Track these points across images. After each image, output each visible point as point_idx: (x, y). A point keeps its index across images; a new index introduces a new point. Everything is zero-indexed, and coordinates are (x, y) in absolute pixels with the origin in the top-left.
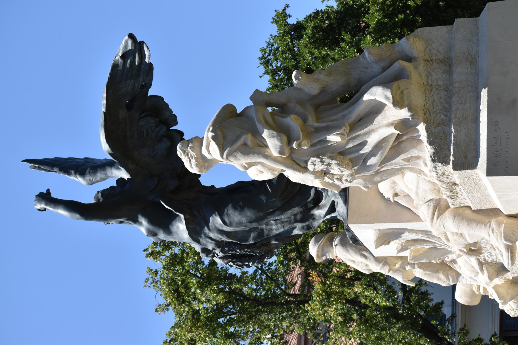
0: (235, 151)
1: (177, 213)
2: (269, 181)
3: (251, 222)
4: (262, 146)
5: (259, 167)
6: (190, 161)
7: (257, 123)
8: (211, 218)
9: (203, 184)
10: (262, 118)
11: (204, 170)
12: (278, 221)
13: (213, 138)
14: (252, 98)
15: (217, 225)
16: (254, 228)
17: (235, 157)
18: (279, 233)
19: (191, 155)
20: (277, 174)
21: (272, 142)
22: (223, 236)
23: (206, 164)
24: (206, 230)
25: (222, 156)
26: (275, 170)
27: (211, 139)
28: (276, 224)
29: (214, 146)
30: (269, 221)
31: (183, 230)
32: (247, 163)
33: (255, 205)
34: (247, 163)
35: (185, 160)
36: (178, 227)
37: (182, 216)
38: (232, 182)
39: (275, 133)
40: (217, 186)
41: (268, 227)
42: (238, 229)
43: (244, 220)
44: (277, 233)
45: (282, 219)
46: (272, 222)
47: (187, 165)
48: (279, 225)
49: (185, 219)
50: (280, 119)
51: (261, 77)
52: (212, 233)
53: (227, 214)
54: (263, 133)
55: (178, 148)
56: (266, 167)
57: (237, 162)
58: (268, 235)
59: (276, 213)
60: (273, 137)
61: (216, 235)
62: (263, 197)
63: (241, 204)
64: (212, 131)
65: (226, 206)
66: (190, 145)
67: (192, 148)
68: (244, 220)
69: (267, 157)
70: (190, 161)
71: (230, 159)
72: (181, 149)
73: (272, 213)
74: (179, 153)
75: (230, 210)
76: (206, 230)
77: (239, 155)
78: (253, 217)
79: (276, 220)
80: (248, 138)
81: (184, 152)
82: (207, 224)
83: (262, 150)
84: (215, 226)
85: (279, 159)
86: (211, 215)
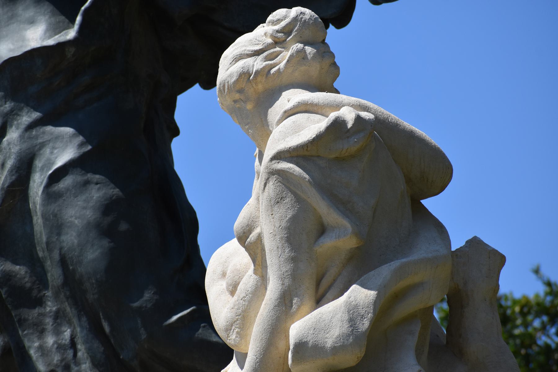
0: (298, 199)
1: (79, 19)
2: (203, 314)
3: (63, 262)
4: (318, 283)
5: (249, 279)
6: (257, 53)
7: (395, 264)
8: (69, 130)
9: (181, 99)
10: (416, 279)
11: (229, 101)
12: (70, 353)
13: (338, 125)
14: (475, 243)
15: (47, 151)
16: (45, 273)
17: (278, 200)
18: (29, 357)
19: (277, 54)
20: (231, 340)
21: (331, 319)
22: (11, 171)
23: (249, 106)
24: (28, 117)
25: (279, 156)
26: (243, 334)
27: (333, 115)
28: (60, 347)
29: (312, 127)
30: (70, 323)
31: (23, 39)
32: (260, 237)
33: (121, 270)
34: (260, 237)
35: (262, 33)
36: (32, 22)
37: (71, 34)
38: (194, 195)
39: (365, 324)
40: (176, 145)
41: (49, 322)
42: (38, 221)
43: (70, 239)
44: (32, 352)
45: (78, 364)
46: (67, 334)
47: (244, 42)
48: (56, 358)
49: (61, 46)
50: (412, 341)
51: (537, 271)
52: (21, 137)
53: (87, 183)
54: (363, 286)
55: (295, 11)
56: (250, 302)
57: (262, 208)
58: (22, 322)
59: (97, 345)
60: (352, 321)
61: (15, 149)
62: (148, 296)
63: (124, 226)
64: (358, 118)
65: (114, 178)
66: (309, 50)
67: (301, 55)
68: (70, 239)
69: (285, 307)
70: (257, 53)
71: (271, 185)
72: (295, 19)
73: (95, 329)
74: (283, 16)
75: (99, 192)
76: (28, 117)
77: (285, 211)
78: (81, 270)
79: (73, 344)
80: (342, 239)
81: (287, 31)
82: (52, 118)
83: (308, 286)
84: (43, 145)
85: (281, 345)
86: (80, 131)
